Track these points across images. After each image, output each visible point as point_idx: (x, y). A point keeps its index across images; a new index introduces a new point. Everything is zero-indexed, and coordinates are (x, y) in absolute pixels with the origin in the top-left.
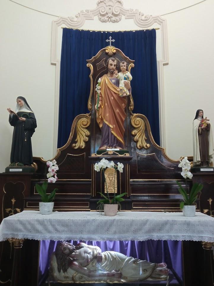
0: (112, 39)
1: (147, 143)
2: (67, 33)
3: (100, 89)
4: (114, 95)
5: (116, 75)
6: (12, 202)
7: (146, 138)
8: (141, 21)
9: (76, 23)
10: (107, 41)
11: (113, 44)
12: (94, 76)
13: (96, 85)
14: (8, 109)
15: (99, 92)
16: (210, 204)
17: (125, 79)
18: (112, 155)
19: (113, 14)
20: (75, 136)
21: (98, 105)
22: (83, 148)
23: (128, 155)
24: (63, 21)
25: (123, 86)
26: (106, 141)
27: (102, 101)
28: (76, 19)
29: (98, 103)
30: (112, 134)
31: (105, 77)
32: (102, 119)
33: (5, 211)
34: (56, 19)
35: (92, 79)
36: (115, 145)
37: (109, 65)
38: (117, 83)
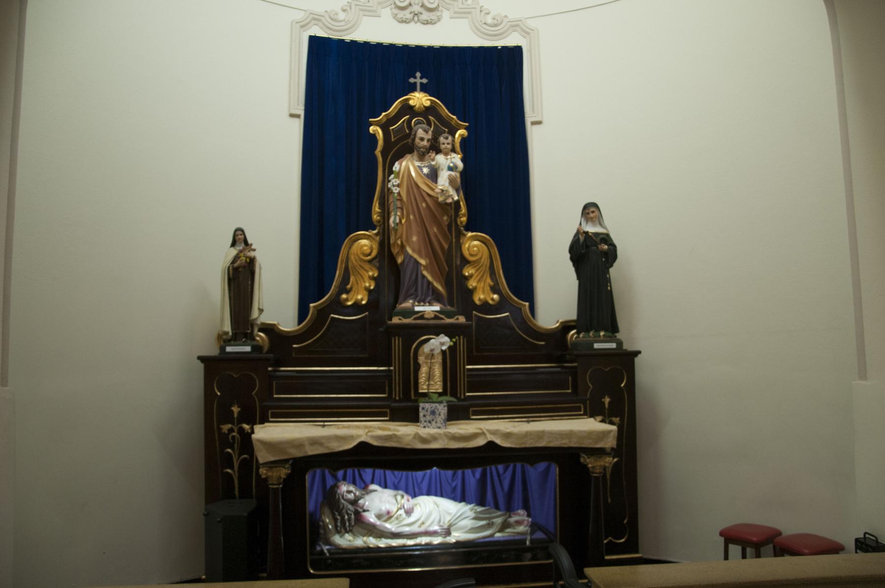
0: (421, 78)
1: (494, 293)
2: (320, 49)
3: (398, 186)
4: (428, 199)
5: (433, 160)
6: (232, 412)
7: (492, 283)
8: (484, 26)
9: (343, 23)
10: (412, 80)
11: (424, 89)
12: (384, 153)
13: (389, 176)
14: (239, 238)
15: (396, 190)
16: (607, 406)
17: (450, 169)
18: (432, 319)
19: (423, 6)
20: (346, 279)
21: (395, 218)
22: (364, 302)
23: (462, 319)
24: (314, 19)
25: (447, 184)
26: (412, 291)
27: (402, 209)
28: (342, 16)
29: (396, 215)
30: (424, 277)
31: (410, 164)
32: (403, 247)
33: (220, 429)
34: (299, 16)
35: (380, 159)
36: (429, 299)
37: (417, 140)
38: (434, 175)
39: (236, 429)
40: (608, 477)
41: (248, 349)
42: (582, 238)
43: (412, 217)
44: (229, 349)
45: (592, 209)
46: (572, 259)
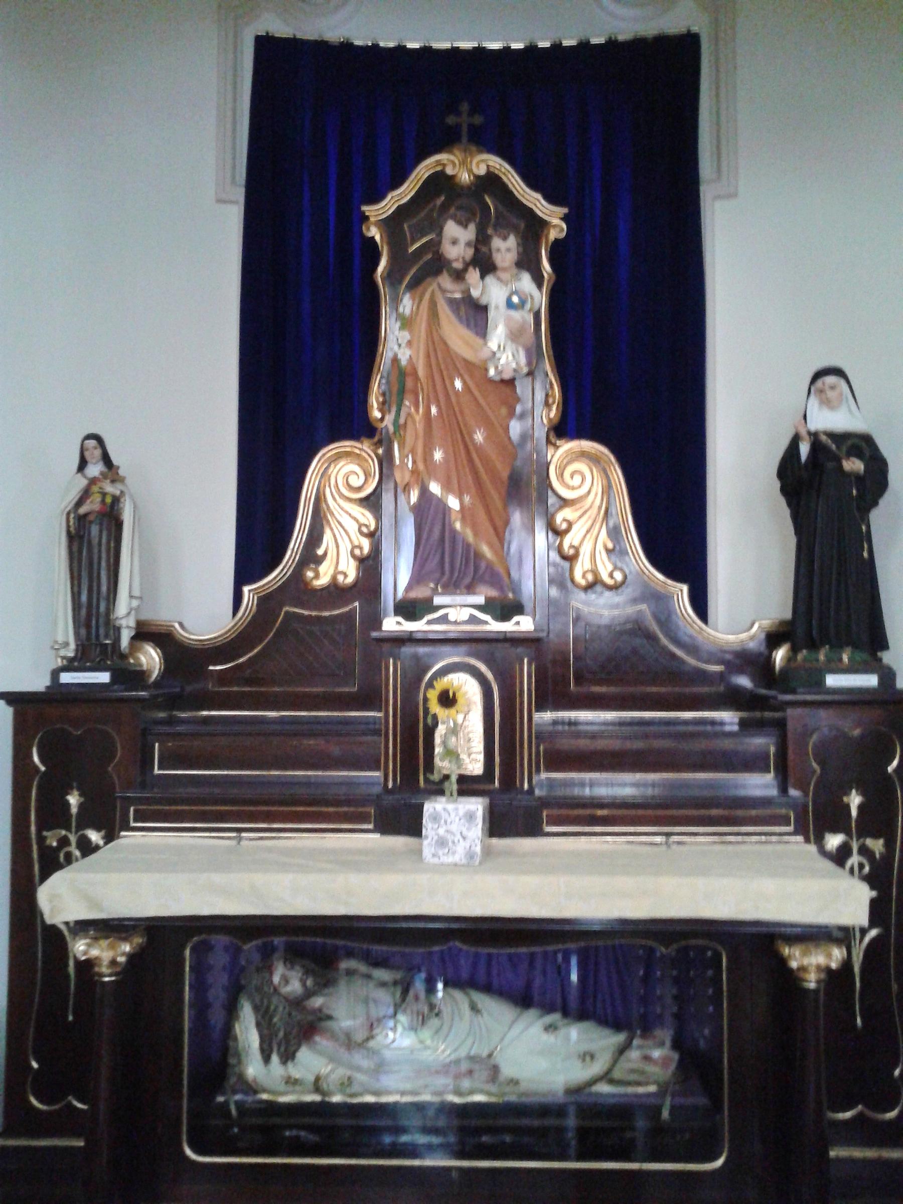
10: (451, 120)
16: (854, 813)
20: (315, 538)
33: (41, 840)
39: (73, 839)
40: (857, 969)
41: (104, 677)
42: (804, 449)
43: (434, 410)
44: (66, 678)
45: (830, 380)
46: (784, 490)
